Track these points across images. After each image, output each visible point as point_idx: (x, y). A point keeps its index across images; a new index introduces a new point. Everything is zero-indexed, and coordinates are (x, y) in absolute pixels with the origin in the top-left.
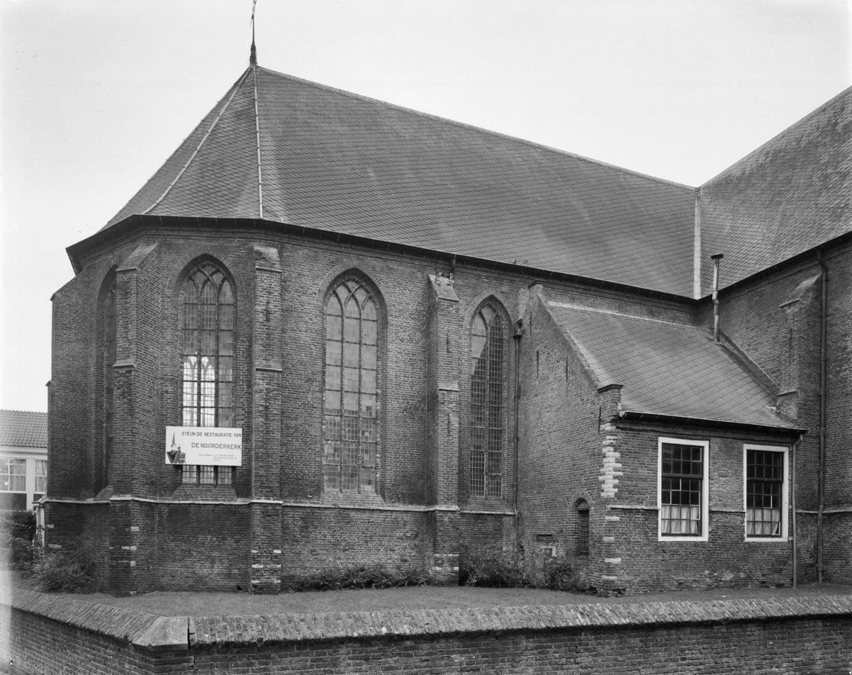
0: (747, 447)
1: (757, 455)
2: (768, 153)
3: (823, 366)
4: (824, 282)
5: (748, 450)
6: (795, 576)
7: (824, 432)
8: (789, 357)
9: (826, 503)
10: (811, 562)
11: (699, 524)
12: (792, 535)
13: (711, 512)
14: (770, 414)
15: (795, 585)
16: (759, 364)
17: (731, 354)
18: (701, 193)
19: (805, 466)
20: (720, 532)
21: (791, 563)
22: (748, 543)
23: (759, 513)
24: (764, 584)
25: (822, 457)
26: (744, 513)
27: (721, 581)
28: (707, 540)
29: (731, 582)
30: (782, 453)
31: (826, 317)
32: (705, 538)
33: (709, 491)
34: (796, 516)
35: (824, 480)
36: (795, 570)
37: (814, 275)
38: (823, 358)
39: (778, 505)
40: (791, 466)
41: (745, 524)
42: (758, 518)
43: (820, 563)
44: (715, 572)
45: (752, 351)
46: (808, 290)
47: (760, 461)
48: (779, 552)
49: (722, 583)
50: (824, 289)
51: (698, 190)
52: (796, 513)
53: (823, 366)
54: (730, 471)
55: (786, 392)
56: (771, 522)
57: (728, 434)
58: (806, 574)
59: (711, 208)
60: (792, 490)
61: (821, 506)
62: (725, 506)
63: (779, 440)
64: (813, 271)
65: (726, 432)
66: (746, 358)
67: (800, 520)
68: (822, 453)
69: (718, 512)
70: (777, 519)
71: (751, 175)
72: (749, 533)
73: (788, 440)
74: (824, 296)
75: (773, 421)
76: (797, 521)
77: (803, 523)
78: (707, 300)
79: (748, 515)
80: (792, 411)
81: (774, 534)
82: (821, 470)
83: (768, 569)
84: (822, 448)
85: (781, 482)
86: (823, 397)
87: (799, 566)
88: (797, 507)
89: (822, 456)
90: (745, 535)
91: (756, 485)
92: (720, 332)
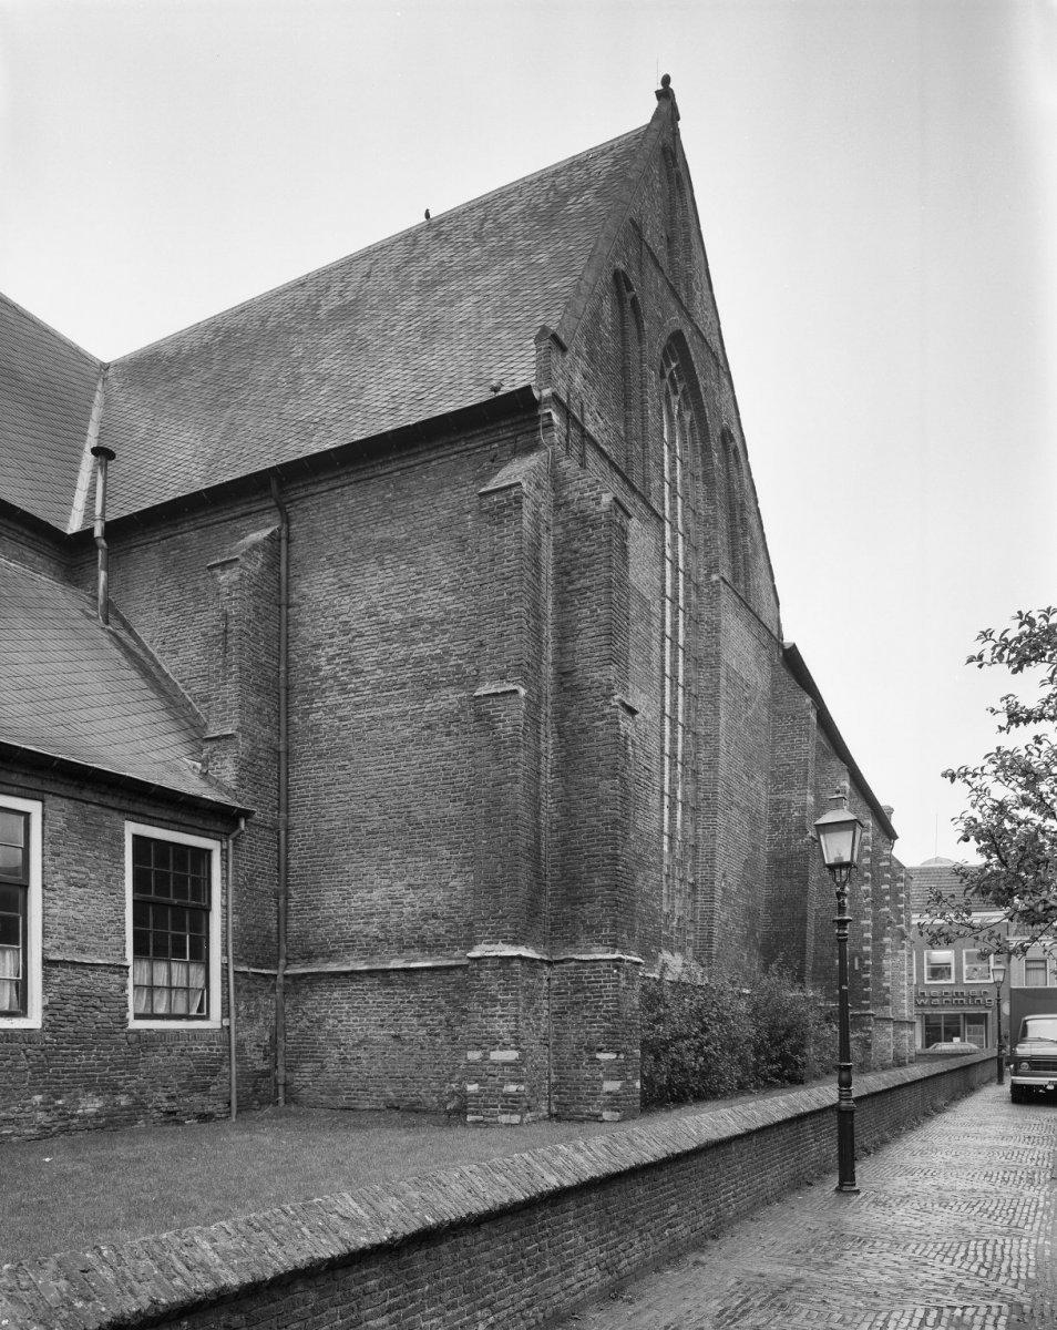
0: (131, 829)
1: (155, 848)
2: (218, 329)
3: (283, 698)
4: (284, 541)
5: (134, 836)
6: (234, 1097)
7: (286, 822)
8: (223, 666)
9: (290, 956)
10: (265, 1067)
11: (21, 988)
12: (228, 1016)
13: (47, 963)
14: (189, 774)
15: (234, 1113)
16: (181, 682)
17: (129, 653)
18: (111, 373)
19: (252, 881)
20: (70, 1008)
21: (227, 1070)
22: (137, 1032)
23: (161, 970)
24: (173, 1118)
25: (282, 869)
26: (128, 967)
27: (73, 1116)
28: (39, 1026)
29: (97, 1116)
30: (209, 852)
31: (288, 607)
32: (34, 1020)
33: (44, 915)
34: (236, 980)
35: (286, 912)
36: (234, 1084)
37: (269, 526)
38: (282, 683)
39: (200, 955)
40: (225, 879)
41: (130, 991)
42: (160, 979)
43: (281, 1068)
44: (59, 1098)
45: (168, 655)
46: (255, 546)
47: (162, 861)
48: (202, 1049)
49: (75, 1121)
50: (284, 554)
51: (106, 367)
52: (235, 972)
53: (283, 698)
54: (92, 876)
55: (217, 734)
56: (187, 989)
57: (87, 795)
58: (256, 1091)
59: (121, 397)
60: (227, 926)
61: (282, 962)
62: (82, 950)
63: (200, 823)
64: (268, 519)
65: (82, 788)
66: (159, 667)
67: (245, 986)
68: (283, 862)
69: (64, 963)
70: (201, 984)
71: (188, 357)
72: (141, 1010)
73: (219, 826)
74: (283, 567)
75: (192, 785)
76: (237, 989)
77: (249, 991)
78: (85, 536)
79: (137, 973)
80: (228, 772)
81: (194, 1012)
82: (282, 894)
83: (180, 1085)
84: (283, 852)
85: (208, 910)
86: (283, 756)
87: (241, 1075)
88: (237, 961)
89: (282, 866)
90: (130, 1015)
91: (173, 914)
92: (108, 604)
